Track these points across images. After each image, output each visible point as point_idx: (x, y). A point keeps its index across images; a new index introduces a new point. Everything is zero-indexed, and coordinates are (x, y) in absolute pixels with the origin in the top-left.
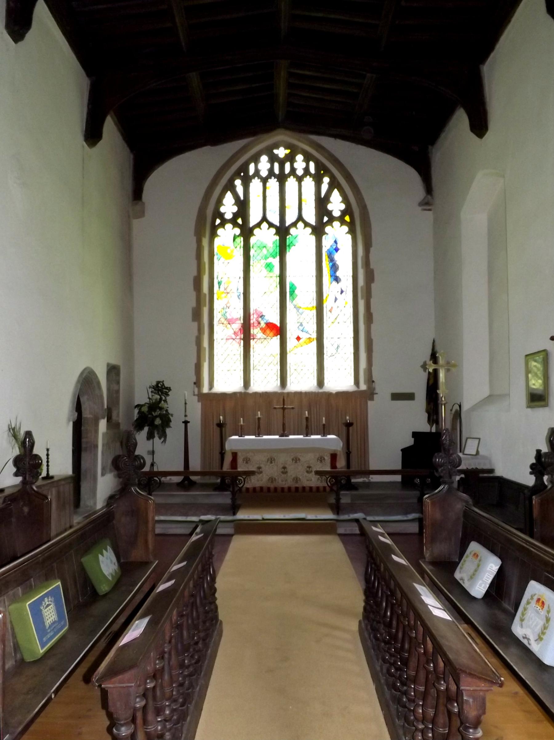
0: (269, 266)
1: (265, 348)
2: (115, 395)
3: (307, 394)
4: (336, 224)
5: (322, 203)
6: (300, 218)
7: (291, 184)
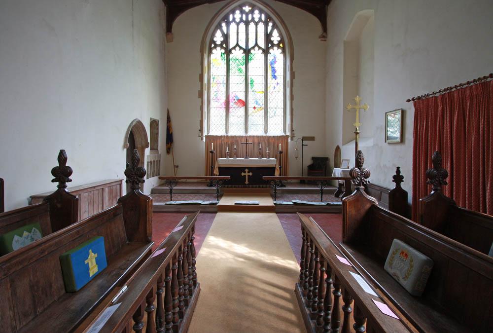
1: (237, 113)
3: (258, 137)
4: (275, 48)
5: (268, 37)
6: (256, 44)
7: (252, 26)
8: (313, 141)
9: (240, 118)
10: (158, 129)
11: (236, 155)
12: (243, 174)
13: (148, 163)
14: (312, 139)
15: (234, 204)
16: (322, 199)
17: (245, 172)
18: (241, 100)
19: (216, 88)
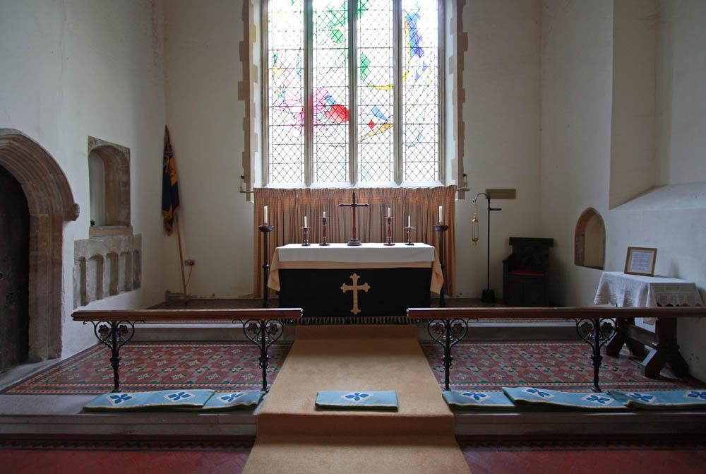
0: (335, 33)
1: (331, 135)
2: (122, 189)
3: (380, 191)
8: (514, 200)
9: (339, 149)
10: (128, 172)
11: (324, 238)
12: (345, 288)
13: (83, 261)
14: (510, 194)
15: (311, 411)
16: (596, 380)
17: (350, 283)
18: (339, 106)
19: (283, 78)
